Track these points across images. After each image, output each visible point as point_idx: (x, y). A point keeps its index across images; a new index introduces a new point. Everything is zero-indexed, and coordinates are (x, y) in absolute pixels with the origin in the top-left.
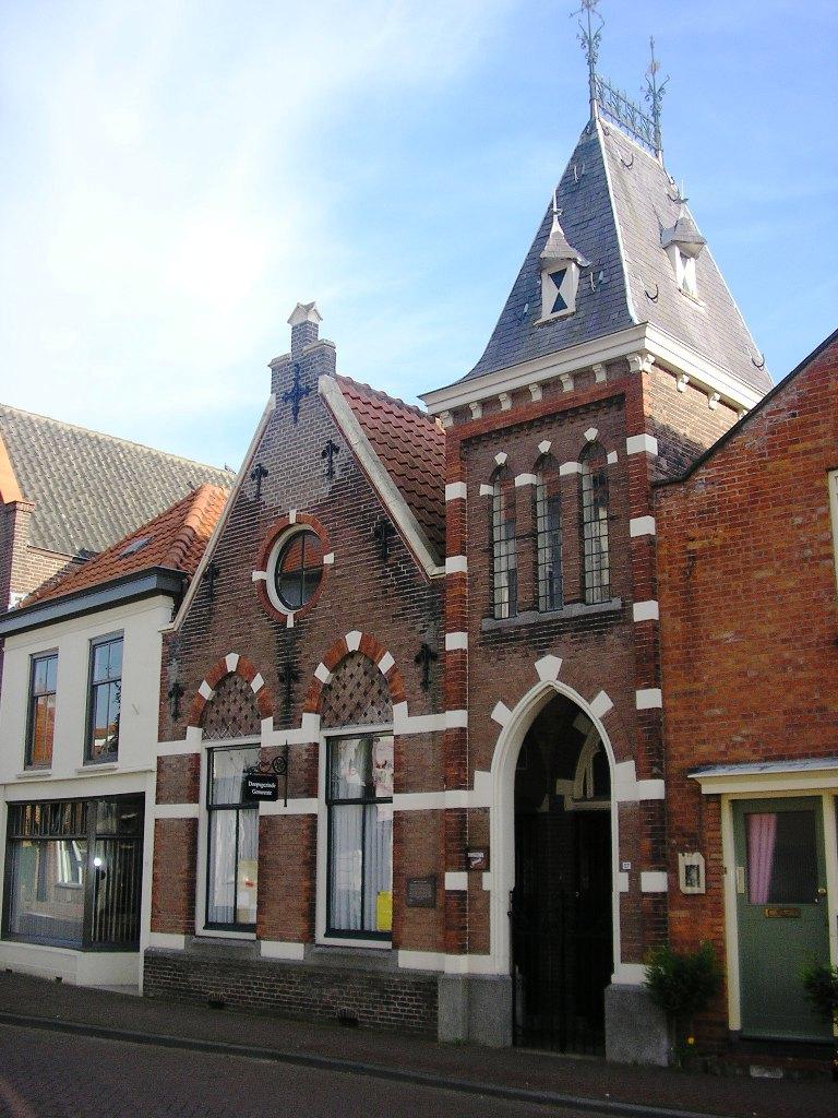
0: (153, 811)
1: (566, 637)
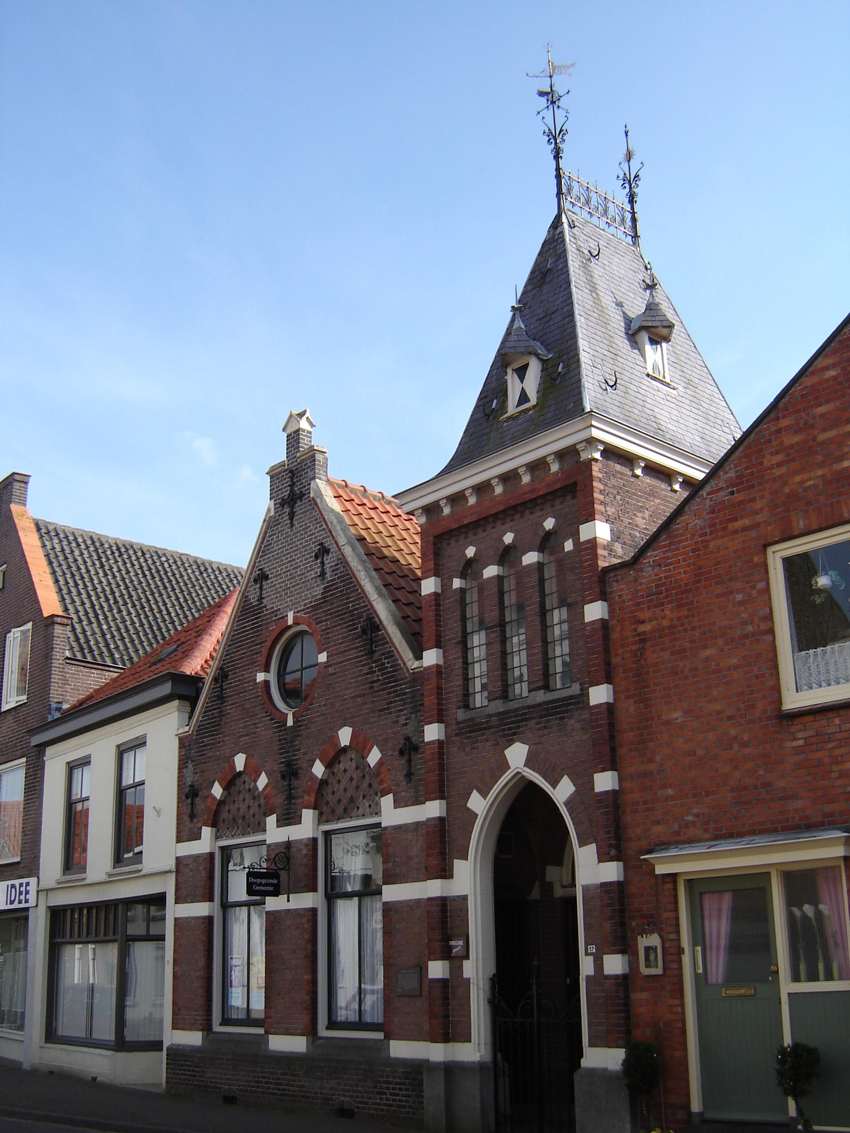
1: (532, 723)
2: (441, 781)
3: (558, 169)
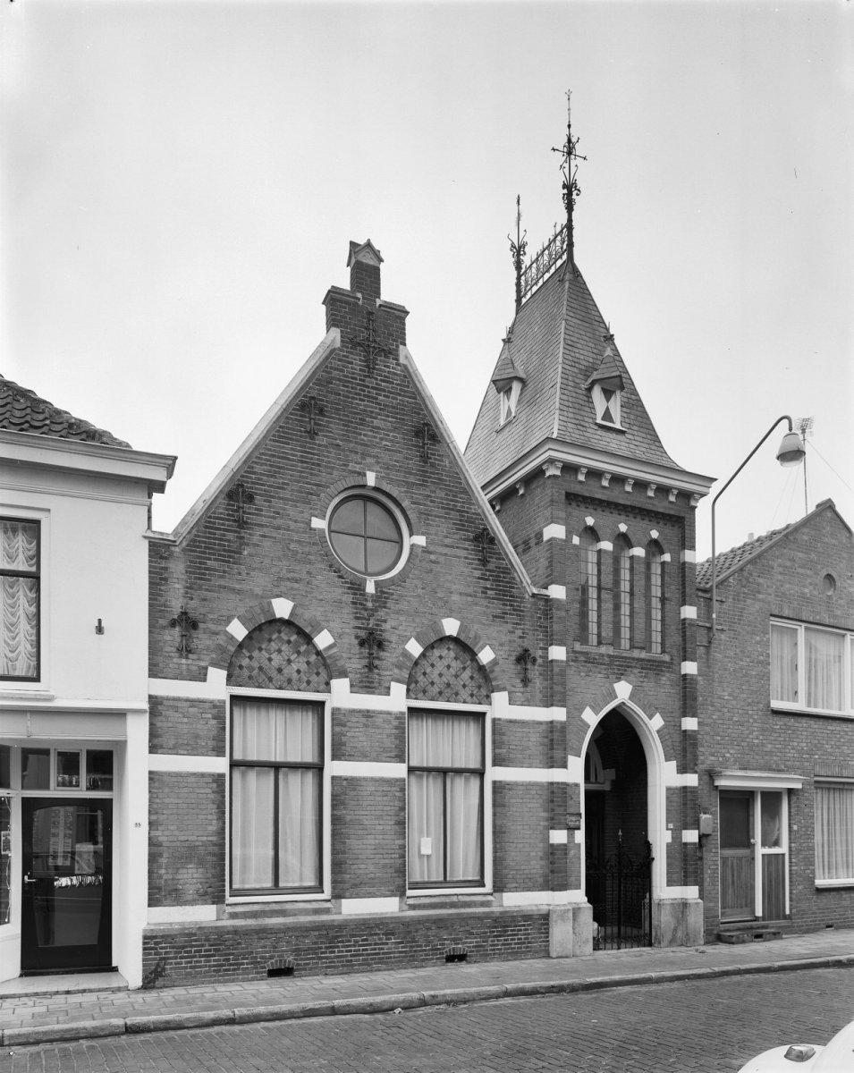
0: (138, 765)
1: (636, 671)
2: (840, 704)
3: (570, 208)
